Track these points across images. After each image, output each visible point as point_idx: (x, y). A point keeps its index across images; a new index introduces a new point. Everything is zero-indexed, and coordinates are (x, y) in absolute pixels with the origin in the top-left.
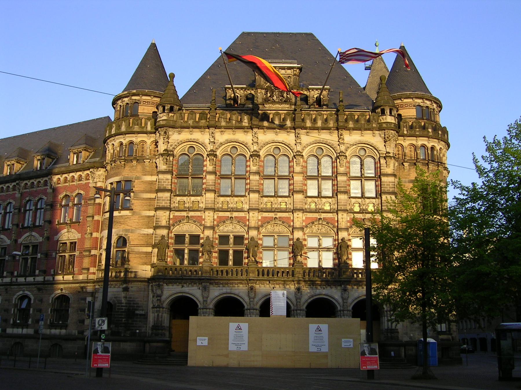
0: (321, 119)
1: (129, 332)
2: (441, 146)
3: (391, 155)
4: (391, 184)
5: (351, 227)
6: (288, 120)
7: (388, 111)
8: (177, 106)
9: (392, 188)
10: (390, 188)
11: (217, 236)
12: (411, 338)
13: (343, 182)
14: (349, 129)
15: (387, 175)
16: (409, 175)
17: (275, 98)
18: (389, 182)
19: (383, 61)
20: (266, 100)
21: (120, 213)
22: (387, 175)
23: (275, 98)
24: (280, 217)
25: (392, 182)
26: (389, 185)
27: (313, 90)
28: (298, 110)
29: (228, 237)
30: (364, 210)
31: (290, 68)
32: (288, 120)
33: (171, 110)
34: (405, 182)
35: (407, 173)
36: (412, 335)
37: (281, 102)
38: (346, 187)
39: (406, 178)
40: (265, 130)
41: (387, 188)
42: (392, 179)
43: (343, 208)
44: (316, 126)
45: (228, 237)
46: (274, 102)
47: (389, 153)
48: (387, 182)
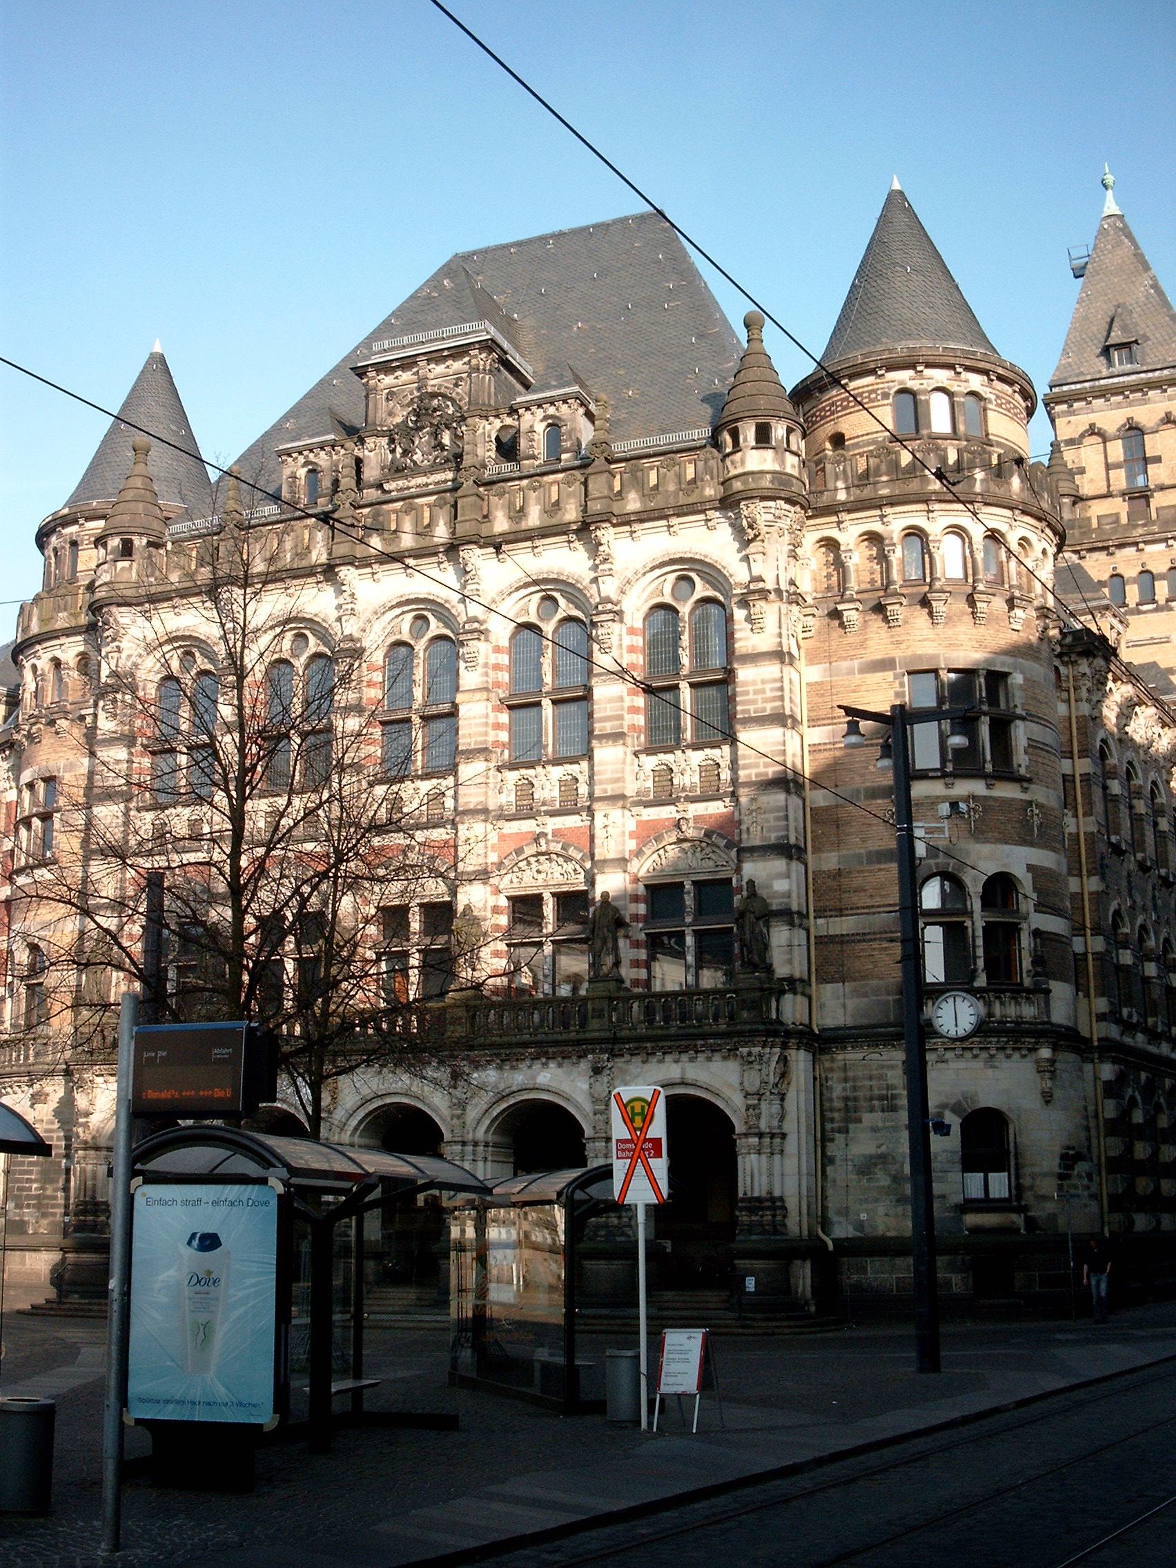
0: (538, 503)
1: (45, 1222)
2: (1021, 532)
3: (770, 585)
4: (768, 687)
5: (638, 853)
6: (441, 522)
7: (748, 433)
8: (141, 534)
9: (774, 699)
10: (765, 701)
11: (504, 903)
12: (860, 1226)
13: (610, 700)
14: (625, 521)
15: (754, 658)
16: (863, 645)
17: (418, 457)
18: (763, 682)
19: (1129, 236)
20: (397, 470)
21: (989, 786)
22: (754, 658)
23: (418, 457)
24: (556, 833)
25: (775, 681)
26: (763, 691)
27: (528, 409)
28: (468, 485)
29: (537, 900)
30: (684, 789)
31: (458, 352)
32: (441, 522)
33: (127, 550)
34: (851, 672)
35: (857, 639)
36: (863, 1216)
37: (433, 469)
38: (621, 718)
39: (852, 658)
40: (375, 566)
41: (754, 702)
42: (771, 670)
43: (610, 790)
44: (524, 525)
45: (537, 900)
46: (416, 470)
47: (760, 579)
48: (754, 683)
